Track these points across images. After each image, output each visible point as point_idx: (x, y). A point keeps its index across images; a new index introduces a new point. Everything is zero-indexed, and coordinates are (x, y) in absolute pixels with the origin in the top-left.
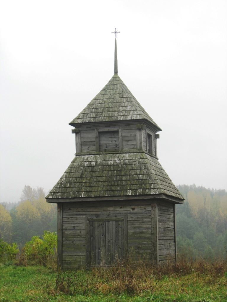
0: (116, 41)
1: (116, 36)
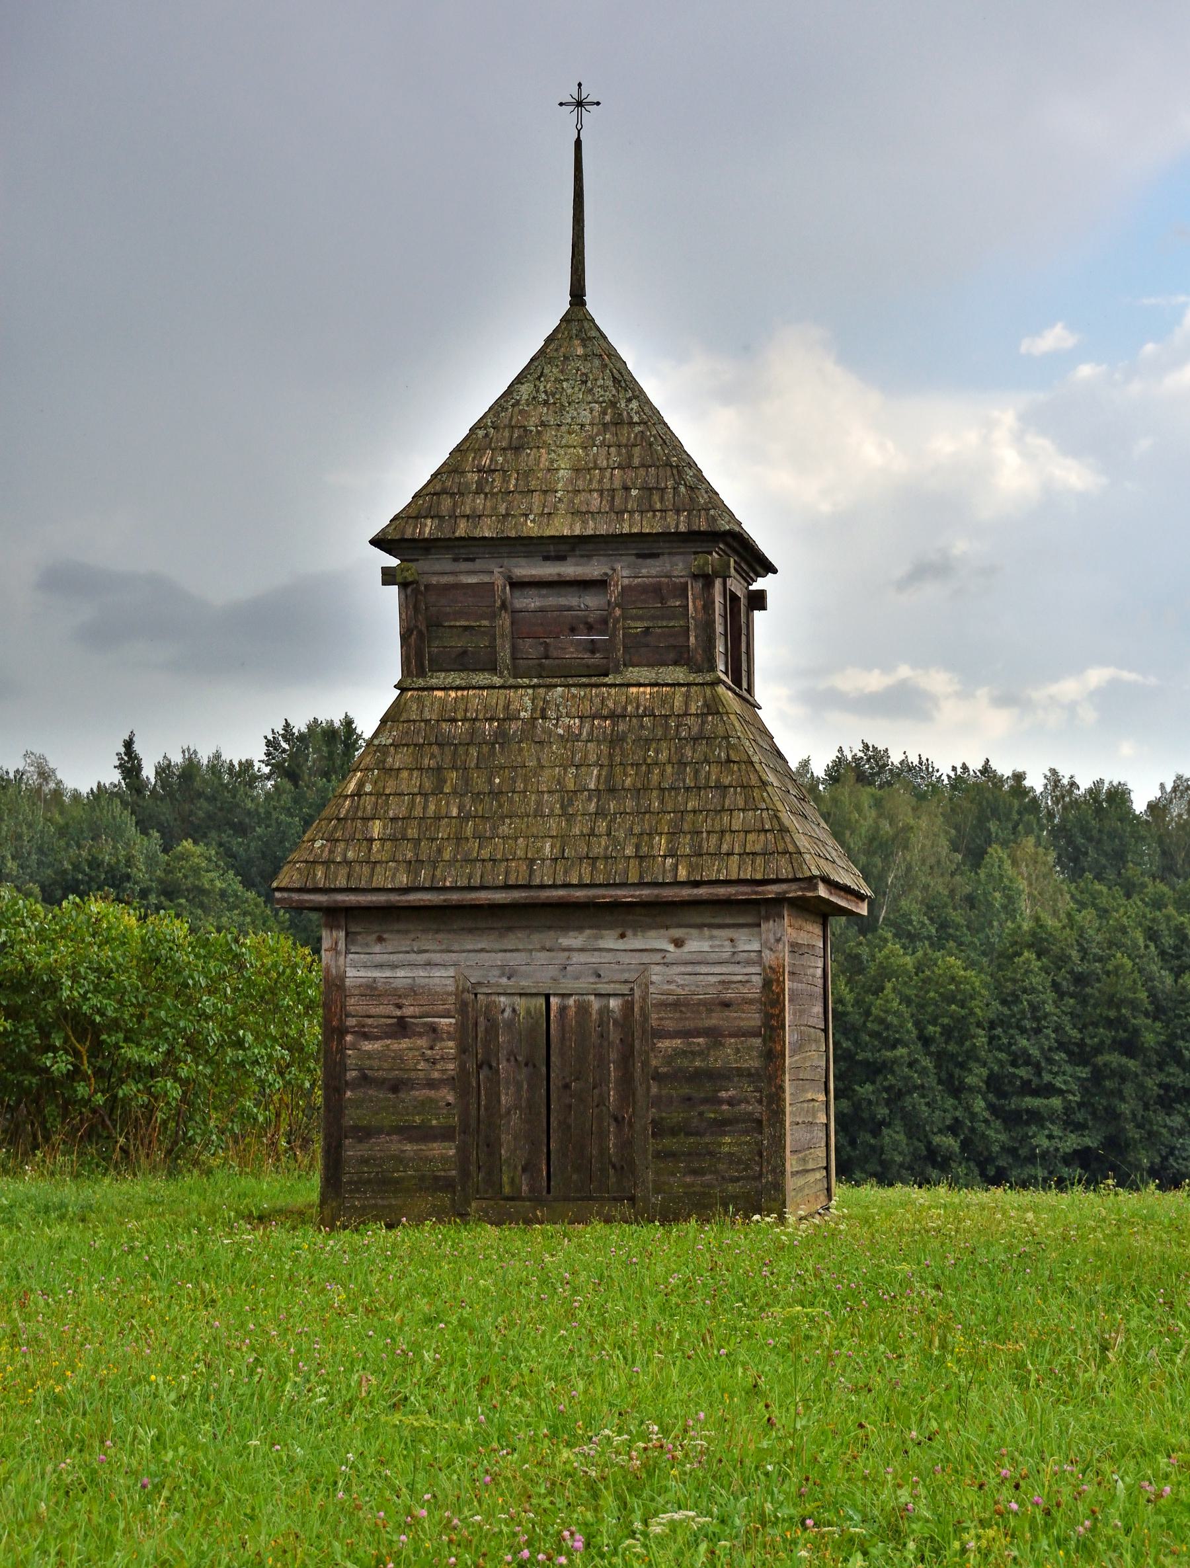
0: (578, 144)
1: (580, 119)
